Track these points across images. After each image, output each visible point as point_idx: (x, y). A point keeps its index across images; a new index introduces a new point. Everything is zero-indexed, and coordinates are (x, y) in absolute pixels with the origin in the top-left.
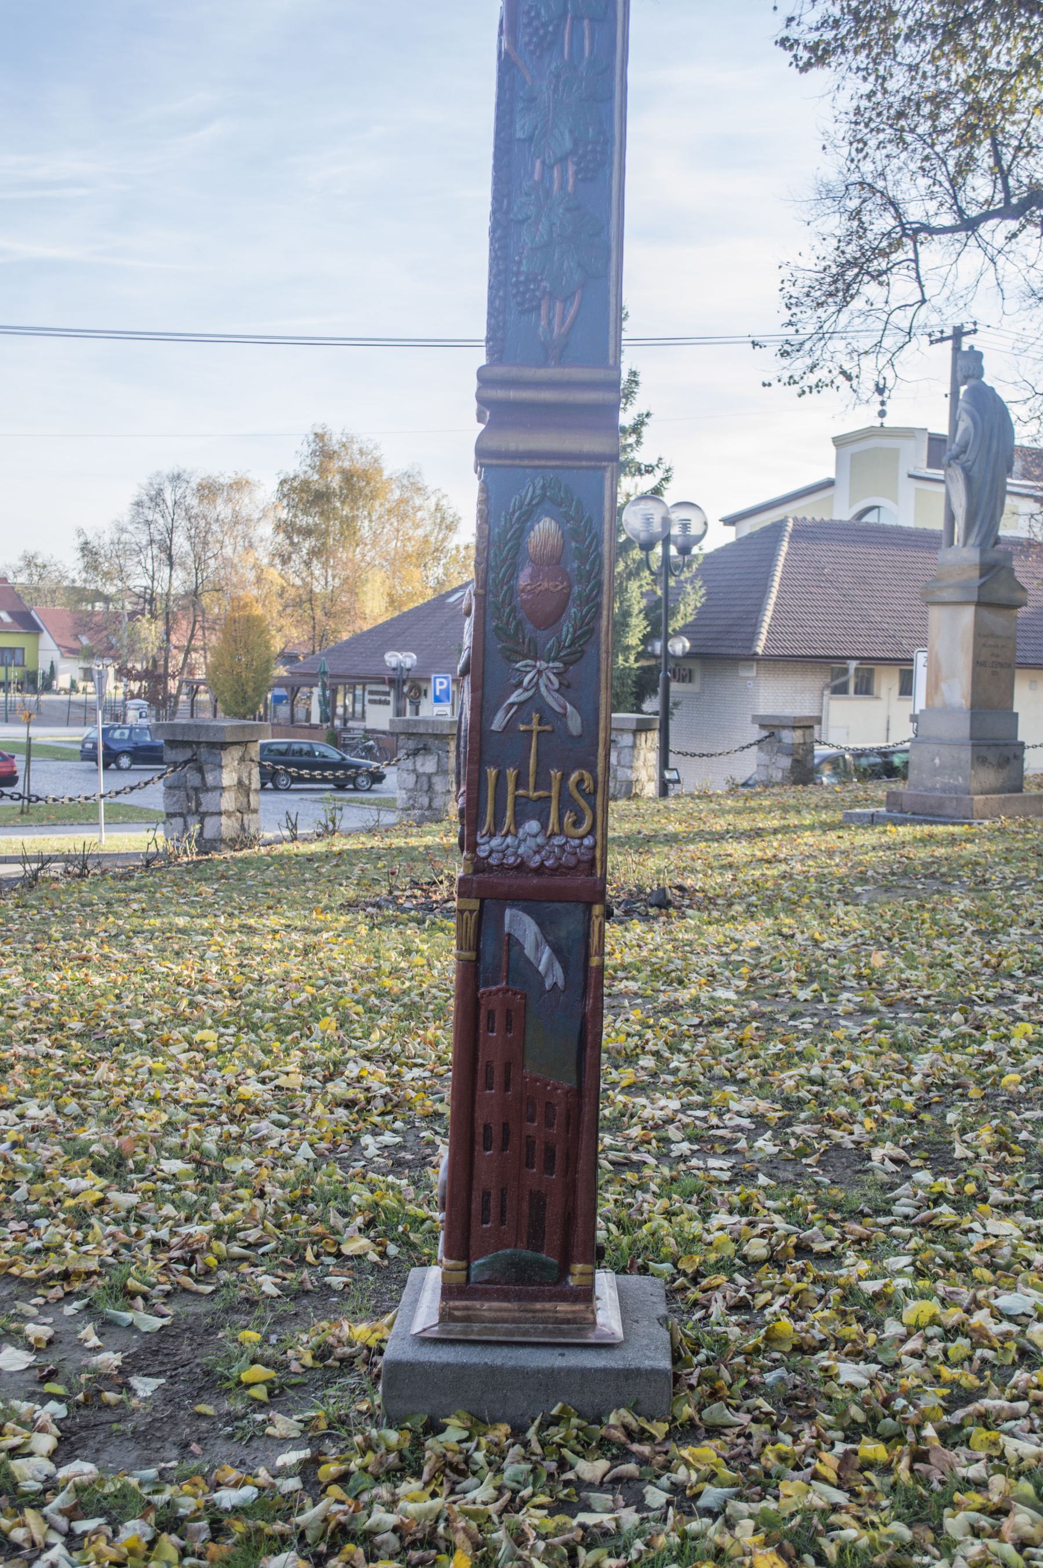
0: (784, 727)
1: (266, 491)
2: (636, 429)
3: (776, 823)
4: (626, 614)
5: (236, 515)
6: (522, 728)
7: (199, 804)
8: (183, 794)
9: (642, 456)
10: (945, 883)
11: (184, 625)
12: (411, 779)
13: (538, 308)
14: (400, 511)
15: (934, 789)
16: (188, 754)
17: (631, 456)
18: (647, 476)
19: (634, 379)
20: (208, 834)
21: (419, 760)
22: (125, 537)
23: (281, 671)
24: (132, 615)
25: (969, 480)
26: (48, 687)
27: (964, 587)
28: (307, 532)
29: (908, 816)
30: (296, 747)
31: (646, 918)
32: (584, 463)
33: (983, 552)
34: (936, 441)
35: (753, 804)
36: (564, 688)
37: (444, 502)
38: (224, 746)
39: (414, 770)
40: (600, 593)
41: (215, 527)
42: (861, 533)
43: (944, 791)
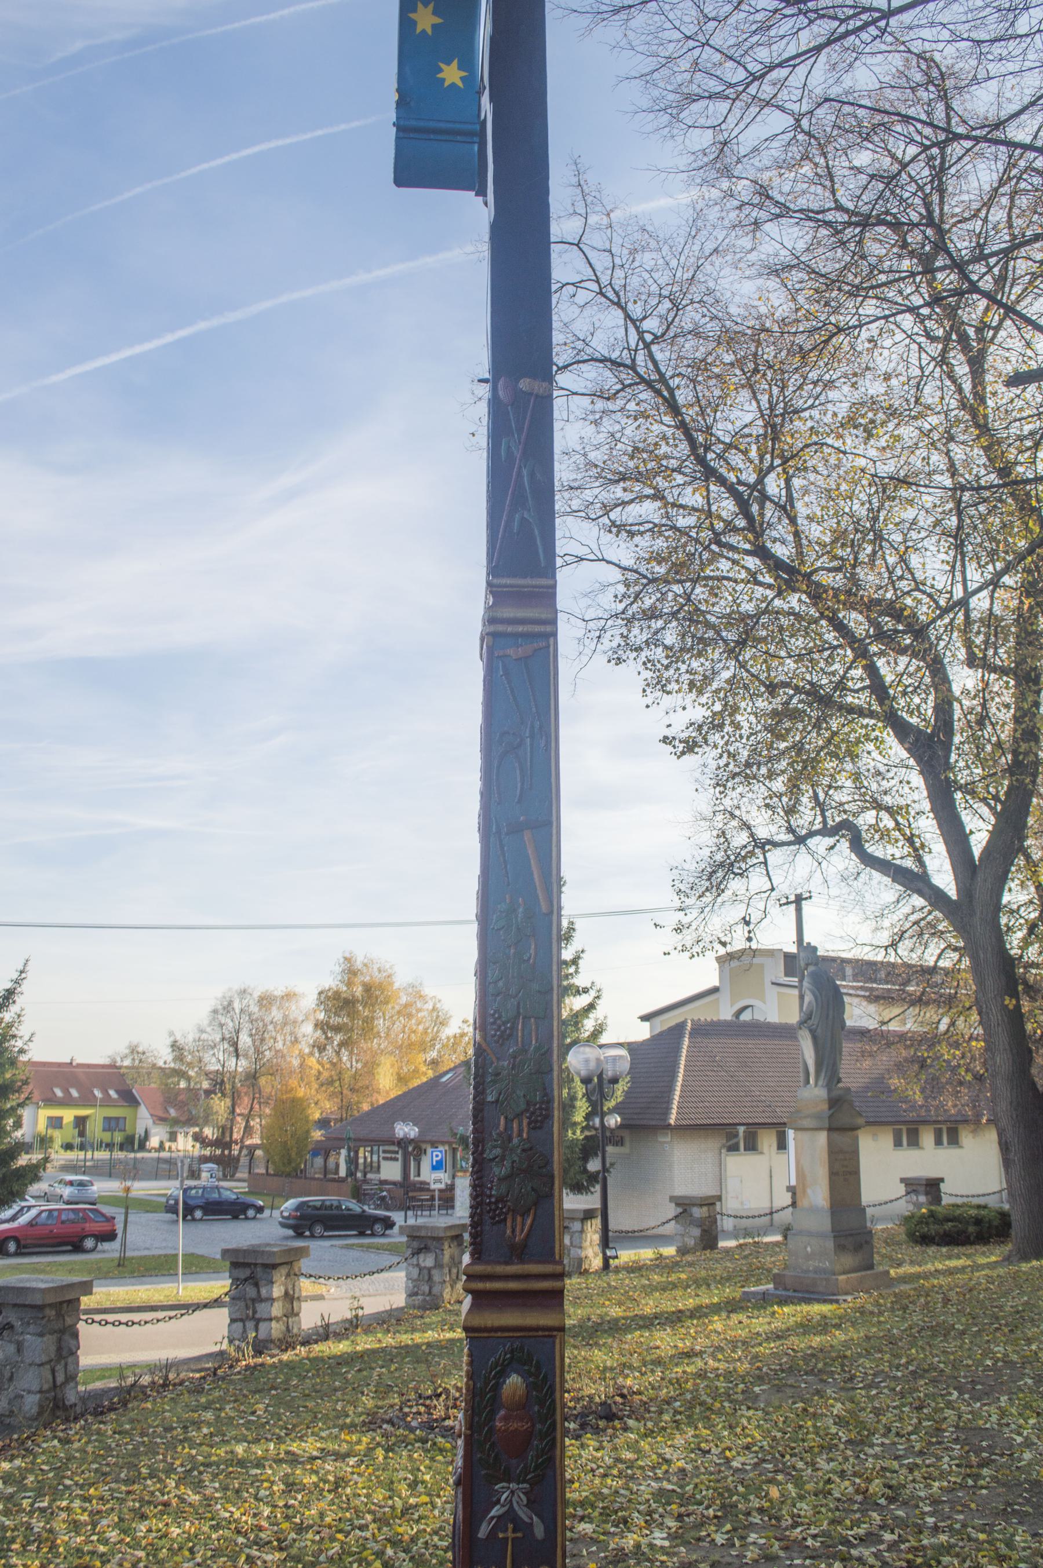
0: (694, 1205)
1: (309, 1000)
2: (575, 961)
3: (691, 1303)
4: (573, 1098)
5: (285, 1016)
6: (501, 1535)
7: (255, 1312)
8: (243, 1304)
9: (580, 981)
10: (822, 1381)
11: (246, 1100)
12: (415, 1272)
13: (505, 1220)
14: (405, 1011)
15: (807, 1271)
16: (247, 1272)
17: (571, 981)
18: (584, 996)
19: (571, 929)
20: (262, 1335)
21: (422, 1256)
22: (204, 1036)
23: (317, 1135)
24: (208, 1093)
25: (815, 1039)
26: (142, 1147)
27: (817, 1117)
28: (337, 1029)
29: (790, 1293)
30: (328, 1203)
31: (597, 1431)
32: (540, 1333)
33: (829, 1091)
34: (789, 957)
35: (673, 1278)
36: (530, 1504)
37: (438, 1005)
38: (274, 1266)
39: (418, 1265)
40: (554, 1429)
41: (270, 1027)
42: (740, 1029)
43: (816, 1272)
